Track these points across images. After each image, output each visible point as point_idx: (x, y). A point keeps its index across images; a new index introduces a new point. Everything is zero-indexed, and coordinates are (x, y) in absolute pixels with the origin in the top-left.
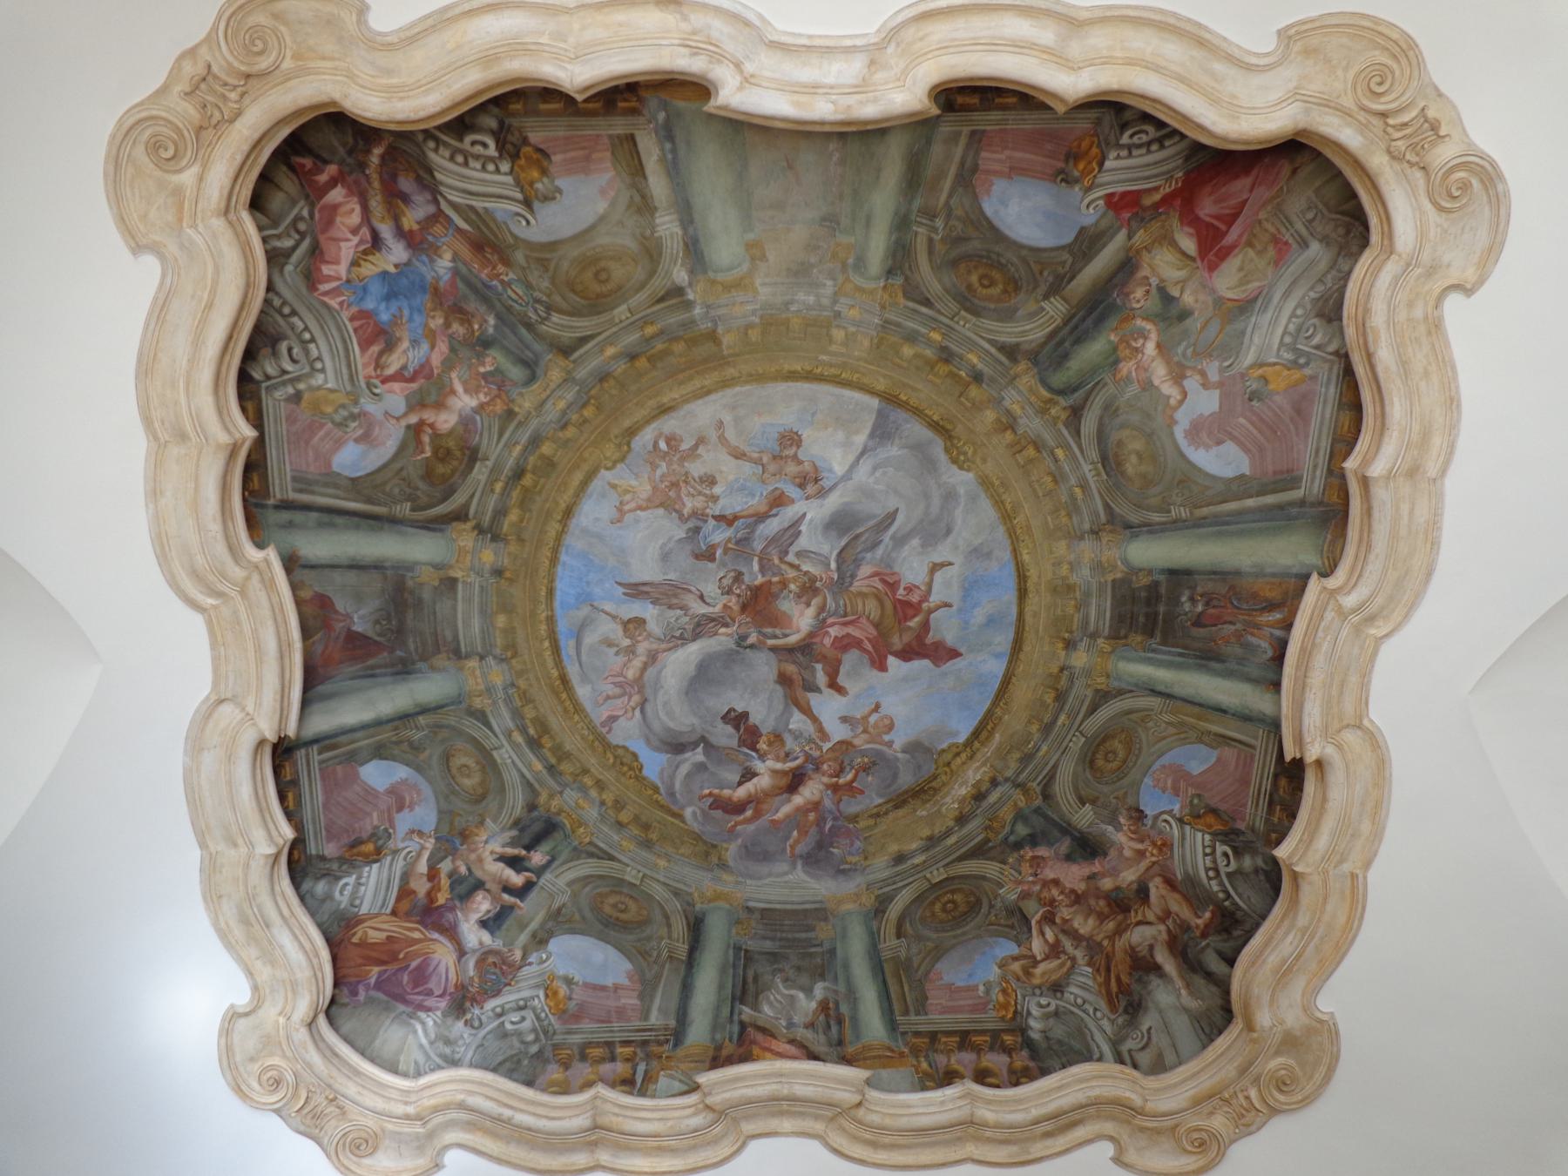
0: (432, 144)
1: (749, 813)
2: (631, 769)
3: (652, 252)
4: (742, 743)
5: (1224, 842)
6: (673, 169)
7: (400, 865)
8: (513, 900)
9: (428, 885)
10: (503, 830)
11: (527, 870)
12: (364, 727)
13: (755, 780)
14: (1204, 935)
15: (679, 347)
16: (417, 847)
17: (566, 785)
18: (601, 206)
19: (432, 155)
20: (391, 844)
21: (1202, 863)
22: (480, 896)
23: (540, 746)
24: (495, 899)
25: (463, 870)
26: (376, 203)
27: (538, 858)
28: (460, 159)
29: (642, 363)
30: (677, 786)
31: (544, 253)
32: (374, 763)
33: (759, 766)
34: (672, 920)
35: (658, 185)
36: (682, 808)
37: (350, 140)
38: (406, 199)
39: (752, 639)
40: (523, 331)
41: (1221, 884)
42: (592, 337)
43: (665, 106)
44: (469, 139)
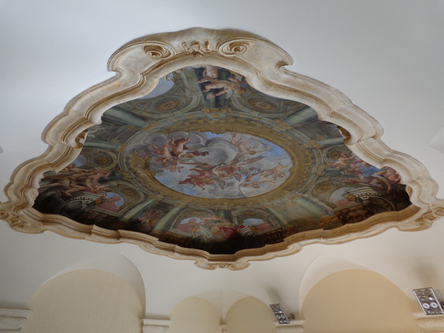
0: (376, 194)
1: (173, 143)
2: (215, 131)
4: (196, 151)
6: (321, 207)
8: (203, 81)
11: (209, 92)
13: (182, 149)
14: (61, 192)
15: (295, 187)
18: (331, 198)
19: (375, 192)
21: (87, 197)
24: (208, 77)
25: (231, 79)
26: (385, 181)
27: (211, 97)
28: (368, 194)
29: (301, 182)
31: (338, 187)
33: (185, 152)
36: (189, 133)
37: (397, 189)
39: (222, 165)
41: (78, 199)
42: (316, 181)
43: (330, 215)
44: (368, 198)
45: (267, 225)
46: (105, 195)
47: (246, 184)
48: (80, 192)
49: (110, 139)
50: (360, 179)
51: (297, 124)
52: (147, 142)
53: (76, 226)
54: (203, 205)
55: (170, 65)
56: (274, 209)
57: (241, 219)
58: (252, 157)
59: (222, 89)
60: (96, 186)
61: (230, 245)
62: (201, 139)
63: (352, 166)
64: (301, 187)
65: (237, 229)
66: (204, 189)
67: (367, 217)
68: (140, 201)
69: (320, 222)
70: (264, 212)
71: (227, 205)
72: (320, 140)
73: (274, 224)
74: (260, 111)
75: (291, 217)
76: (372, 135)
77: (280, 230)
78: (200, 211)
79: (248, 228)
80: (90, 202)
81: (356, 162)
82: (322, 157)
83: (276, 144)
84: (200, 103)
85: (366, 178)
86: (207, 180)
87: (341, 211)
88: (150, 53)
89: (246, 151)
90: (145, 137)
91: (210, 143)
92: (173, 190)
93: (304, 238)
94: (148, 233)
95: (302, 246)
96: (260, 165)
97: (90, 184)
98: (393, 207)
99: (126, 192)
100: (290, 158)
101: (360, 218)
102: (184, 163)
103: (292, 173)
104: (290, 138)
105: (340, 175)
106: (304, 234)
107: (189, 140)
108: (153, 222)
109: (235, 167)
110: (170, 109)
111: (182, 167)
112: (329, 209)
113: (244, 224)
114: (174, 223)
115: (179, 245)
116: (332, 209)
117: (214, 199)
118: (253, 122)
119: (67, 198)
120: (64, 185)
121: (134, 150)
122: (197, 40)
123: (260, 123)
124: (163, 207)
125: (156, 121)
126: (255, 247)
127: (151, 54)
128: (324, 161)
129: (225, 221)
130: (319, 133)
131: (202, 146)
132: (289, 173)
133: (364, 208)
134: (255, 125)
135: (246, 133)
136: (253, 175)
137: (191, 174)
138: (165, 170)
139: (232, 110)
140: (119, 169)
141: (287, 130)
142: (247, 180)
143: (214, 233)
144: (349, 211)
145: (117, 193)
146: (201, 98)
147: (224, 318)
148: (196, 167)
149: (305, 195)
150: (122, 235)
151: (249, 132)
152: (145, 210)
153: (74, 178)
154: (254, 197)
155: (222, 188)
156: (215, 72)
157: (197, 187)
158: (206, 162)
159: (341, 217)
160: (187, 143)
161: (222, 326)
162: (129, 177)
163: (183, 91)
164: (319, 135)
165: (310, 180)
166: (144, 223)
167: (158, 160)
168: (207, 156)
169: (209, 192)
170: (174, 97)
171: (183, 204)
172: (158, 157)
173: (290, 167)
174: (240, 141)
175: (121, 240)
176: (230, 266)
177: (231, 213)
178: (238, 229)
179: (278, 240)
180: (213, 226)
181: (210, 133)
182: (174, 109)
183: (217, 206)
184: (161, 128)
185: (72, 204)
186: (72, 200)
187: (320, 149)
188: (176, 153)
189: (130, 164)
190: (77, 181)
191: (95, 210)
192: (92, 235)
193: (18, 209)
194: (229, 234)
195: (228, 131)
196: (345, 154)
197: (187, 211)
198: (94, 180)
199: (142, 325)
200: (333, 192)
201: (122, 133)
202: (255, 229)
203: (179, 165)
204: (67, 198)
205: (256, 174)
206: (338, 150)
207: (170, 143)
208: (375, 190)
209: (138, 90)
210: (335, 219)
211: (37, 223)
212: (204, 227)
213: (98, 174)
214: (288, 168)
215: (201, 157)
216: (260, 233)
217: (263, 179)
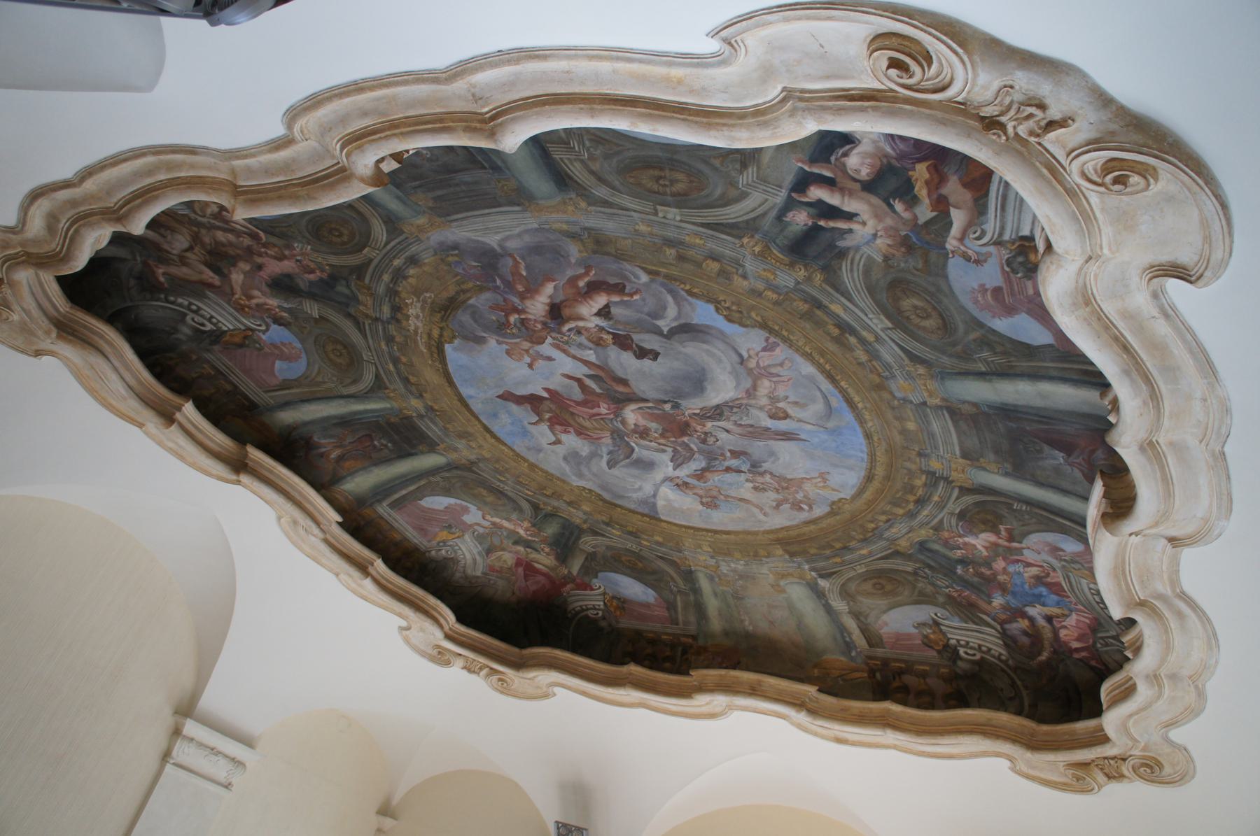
1: (581, 284)
3: (845, 593)
4: (628, 337)
5: (212, 332)
6: (842, 629)
7: (991, 225)
9: (945, 191)
10: (857, 249)
11: (809, 204)
12: (1051, 379)
13: (595, 310)
14: (145, 264)
15: (813, 551)
16: (967, 241)
17: (795, 290)
18: (885, 617)
19: (1004, 652)
20: (1005, 254)
21: (207, 311)
22: (865, 173)
23: (838, 326)
25: (899, 206)
27: (800, 219)
29: (838, 545)
30: (670, 299)
31: (922, 599)
32: (1035, 343)
34: (592, 178)
35: (851, 624)
36: (652, 281)
38: (1025, 633)
40: (932, 564)
41: (180, 305)
43: (852, 659)
44: (978, 657)
45: (662, 612)
46: (263, 328)
47: (686, 484)
48: (199, 289)
49: (415, 188)
50: (990, 603)
51: (964, 402)
52: (512, 245)
53: (141, 383)
54: (520, 483)
55: (892, 114)
56: (711, 579)
57: (595, 564)
58: (769, 423)
59: (850, 216)
60: (256, 293)
61: (518, 622)
62: (672, 311)
63: (999, 564)
64: (828, 558)
65: (565, 585)
66: (558, 442)
67: (948, 707)
68: (352, 390)
69: (815, 666)
70: (675, 575)
71: (585, 513)
72: (984, 469)
73: (681, 618)
74: (899, 320)
75: (742, 621)
76: (1173, 533)
77: (690, 640)
78: (500, 493)
79: (601, 598)
80: (209, 327)
81: (1018, 561)
82: (946, 510)
83: (861, 421)
84: (754, 219)
85: (1005, 608)
86: (587, 424)
87: (886, 662)
88: (883, 57)
89: (764, 401)
90: (517, 231)
91: (686, 332)
92: (467, 406)
93: (754, 691)
94: (319, 487)
95: (731, 708)
96: (772, 454)
97: (242, 277)
98: (1026, 704)
99: (329, 348)
100: (863, 473)
101: (926, 700)
102: (564, 351)
103: (832, 513)
104: (911, 426)
105: (949, 572)
106: (759, 682)
107: (635, 297)
108: (347, 464)
109: (699, 428)
110: (658, 193)
111: (550, 359)
112: (861, 642)
113: (596, 583)
114: (404, 492)
115: (386, 561)
116: (867, 646)
117: (564, 481)
118: (853, 340)
119: (150, 287)
120: (166, 247)
121: (455, 247)
122: (1048, 101)
123: (867, 351)
124: (403, 436)
125: (589, 204)
126: (590, 656)
127: (885, 64)
128: (941, 521)
129: (547, 550)
130: (997, 452)
131: (658, 332)
132: (827, 509)
133: (952, 678)
134: (851, 350)
135: (808, 356)
136: (728, 469)
137: (559, 389)
138: (492, 342)
139: (826, 281)
140: (360, 277)
141: (925, 403)
142: (700, 475)
143: (492, 569)
144: (908, 668)
145: (302, 341)
146: (772, 208)
147: (394, 802)
148: (589, 376)
149: (823, 583)
150: (250, 464)
151: (817, 357)
152: (344, 422)
153: (207, 240)
154: (682, 526)
155: (611, 464)
156: (872, 166)
157: (544, 427)
158: (629, 377)
159: (878, 675)
160: (622, 302)
161: (382, 818)
162: (370, 312)
163: (738, 166)
164: (992, 456)
165: (864, 552)
166: (322, 455)
167: (495, 307)
168: (647, 363)
169: (565, 458)
170: (702, 167)
171: (465, 452)
172: (505, 300)
173: (842, 496)
174: (773, 370)
175: (245, 478)
176: (495, 677)
177: (578, 538)
178: (569, 587)
179: (667, 665)
180: (503, 550)
181: (711, 307)
182: (670, 198)
183: (556, 504)
184: (585, 229)
185: (153, 311)
186: (158, 300)
187: (961, 488)
188: (566, 312)
189: (405, 278)
190: (210, 252)
191: (208, 356)
192: (174, 427)
193: (23, 262)
194: (533, 588)
195: (764, 326)
196: (1009, 531)
197: (464, 478)
198: (261, 273)
199: (177, 732)
200: (900, 605)
201: (464, 188)
202: (618, 608)
203: (546, 348)
204: (150, 287)
205: (739, 471)
206: (1004, 512)
207: (573, 281)
208: (1006, 645)
209: (724, 125)
210: (858, 675)
211: (45, 323)
212: (474, 537)
213: (286, 262)
214: (835, 496)
215: (627, 358)
216: (625, 623)
217: (746, 491)
